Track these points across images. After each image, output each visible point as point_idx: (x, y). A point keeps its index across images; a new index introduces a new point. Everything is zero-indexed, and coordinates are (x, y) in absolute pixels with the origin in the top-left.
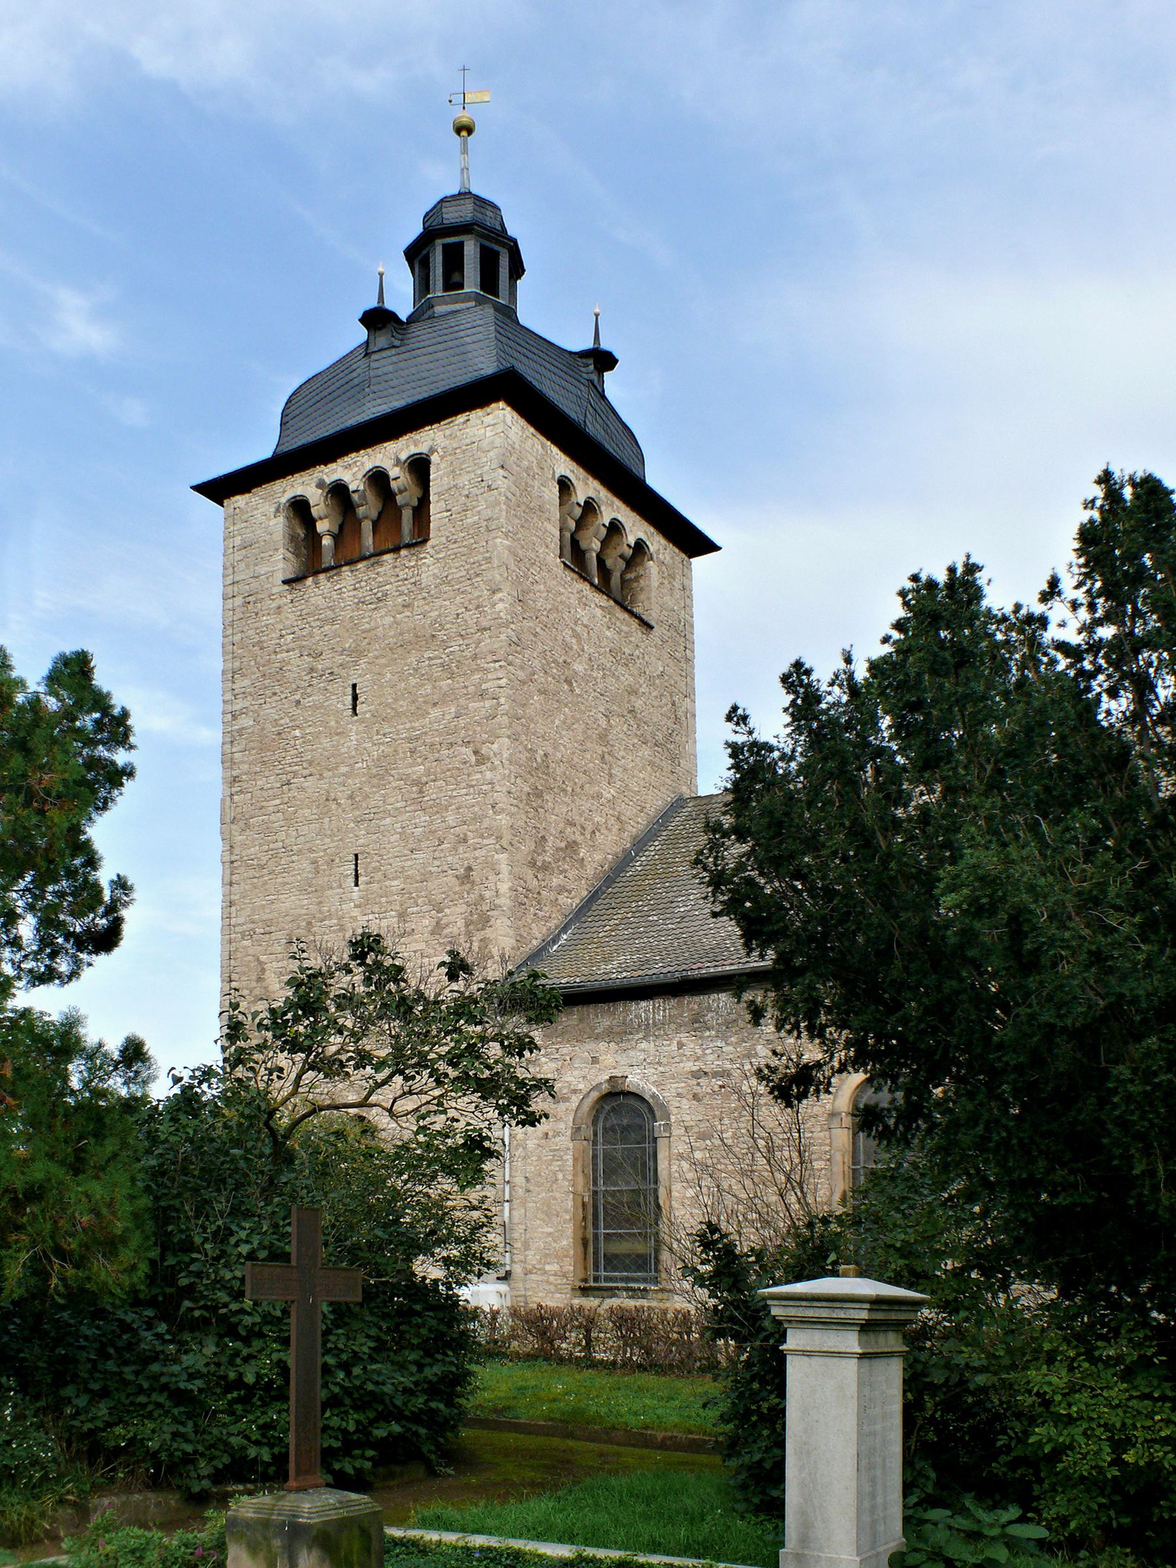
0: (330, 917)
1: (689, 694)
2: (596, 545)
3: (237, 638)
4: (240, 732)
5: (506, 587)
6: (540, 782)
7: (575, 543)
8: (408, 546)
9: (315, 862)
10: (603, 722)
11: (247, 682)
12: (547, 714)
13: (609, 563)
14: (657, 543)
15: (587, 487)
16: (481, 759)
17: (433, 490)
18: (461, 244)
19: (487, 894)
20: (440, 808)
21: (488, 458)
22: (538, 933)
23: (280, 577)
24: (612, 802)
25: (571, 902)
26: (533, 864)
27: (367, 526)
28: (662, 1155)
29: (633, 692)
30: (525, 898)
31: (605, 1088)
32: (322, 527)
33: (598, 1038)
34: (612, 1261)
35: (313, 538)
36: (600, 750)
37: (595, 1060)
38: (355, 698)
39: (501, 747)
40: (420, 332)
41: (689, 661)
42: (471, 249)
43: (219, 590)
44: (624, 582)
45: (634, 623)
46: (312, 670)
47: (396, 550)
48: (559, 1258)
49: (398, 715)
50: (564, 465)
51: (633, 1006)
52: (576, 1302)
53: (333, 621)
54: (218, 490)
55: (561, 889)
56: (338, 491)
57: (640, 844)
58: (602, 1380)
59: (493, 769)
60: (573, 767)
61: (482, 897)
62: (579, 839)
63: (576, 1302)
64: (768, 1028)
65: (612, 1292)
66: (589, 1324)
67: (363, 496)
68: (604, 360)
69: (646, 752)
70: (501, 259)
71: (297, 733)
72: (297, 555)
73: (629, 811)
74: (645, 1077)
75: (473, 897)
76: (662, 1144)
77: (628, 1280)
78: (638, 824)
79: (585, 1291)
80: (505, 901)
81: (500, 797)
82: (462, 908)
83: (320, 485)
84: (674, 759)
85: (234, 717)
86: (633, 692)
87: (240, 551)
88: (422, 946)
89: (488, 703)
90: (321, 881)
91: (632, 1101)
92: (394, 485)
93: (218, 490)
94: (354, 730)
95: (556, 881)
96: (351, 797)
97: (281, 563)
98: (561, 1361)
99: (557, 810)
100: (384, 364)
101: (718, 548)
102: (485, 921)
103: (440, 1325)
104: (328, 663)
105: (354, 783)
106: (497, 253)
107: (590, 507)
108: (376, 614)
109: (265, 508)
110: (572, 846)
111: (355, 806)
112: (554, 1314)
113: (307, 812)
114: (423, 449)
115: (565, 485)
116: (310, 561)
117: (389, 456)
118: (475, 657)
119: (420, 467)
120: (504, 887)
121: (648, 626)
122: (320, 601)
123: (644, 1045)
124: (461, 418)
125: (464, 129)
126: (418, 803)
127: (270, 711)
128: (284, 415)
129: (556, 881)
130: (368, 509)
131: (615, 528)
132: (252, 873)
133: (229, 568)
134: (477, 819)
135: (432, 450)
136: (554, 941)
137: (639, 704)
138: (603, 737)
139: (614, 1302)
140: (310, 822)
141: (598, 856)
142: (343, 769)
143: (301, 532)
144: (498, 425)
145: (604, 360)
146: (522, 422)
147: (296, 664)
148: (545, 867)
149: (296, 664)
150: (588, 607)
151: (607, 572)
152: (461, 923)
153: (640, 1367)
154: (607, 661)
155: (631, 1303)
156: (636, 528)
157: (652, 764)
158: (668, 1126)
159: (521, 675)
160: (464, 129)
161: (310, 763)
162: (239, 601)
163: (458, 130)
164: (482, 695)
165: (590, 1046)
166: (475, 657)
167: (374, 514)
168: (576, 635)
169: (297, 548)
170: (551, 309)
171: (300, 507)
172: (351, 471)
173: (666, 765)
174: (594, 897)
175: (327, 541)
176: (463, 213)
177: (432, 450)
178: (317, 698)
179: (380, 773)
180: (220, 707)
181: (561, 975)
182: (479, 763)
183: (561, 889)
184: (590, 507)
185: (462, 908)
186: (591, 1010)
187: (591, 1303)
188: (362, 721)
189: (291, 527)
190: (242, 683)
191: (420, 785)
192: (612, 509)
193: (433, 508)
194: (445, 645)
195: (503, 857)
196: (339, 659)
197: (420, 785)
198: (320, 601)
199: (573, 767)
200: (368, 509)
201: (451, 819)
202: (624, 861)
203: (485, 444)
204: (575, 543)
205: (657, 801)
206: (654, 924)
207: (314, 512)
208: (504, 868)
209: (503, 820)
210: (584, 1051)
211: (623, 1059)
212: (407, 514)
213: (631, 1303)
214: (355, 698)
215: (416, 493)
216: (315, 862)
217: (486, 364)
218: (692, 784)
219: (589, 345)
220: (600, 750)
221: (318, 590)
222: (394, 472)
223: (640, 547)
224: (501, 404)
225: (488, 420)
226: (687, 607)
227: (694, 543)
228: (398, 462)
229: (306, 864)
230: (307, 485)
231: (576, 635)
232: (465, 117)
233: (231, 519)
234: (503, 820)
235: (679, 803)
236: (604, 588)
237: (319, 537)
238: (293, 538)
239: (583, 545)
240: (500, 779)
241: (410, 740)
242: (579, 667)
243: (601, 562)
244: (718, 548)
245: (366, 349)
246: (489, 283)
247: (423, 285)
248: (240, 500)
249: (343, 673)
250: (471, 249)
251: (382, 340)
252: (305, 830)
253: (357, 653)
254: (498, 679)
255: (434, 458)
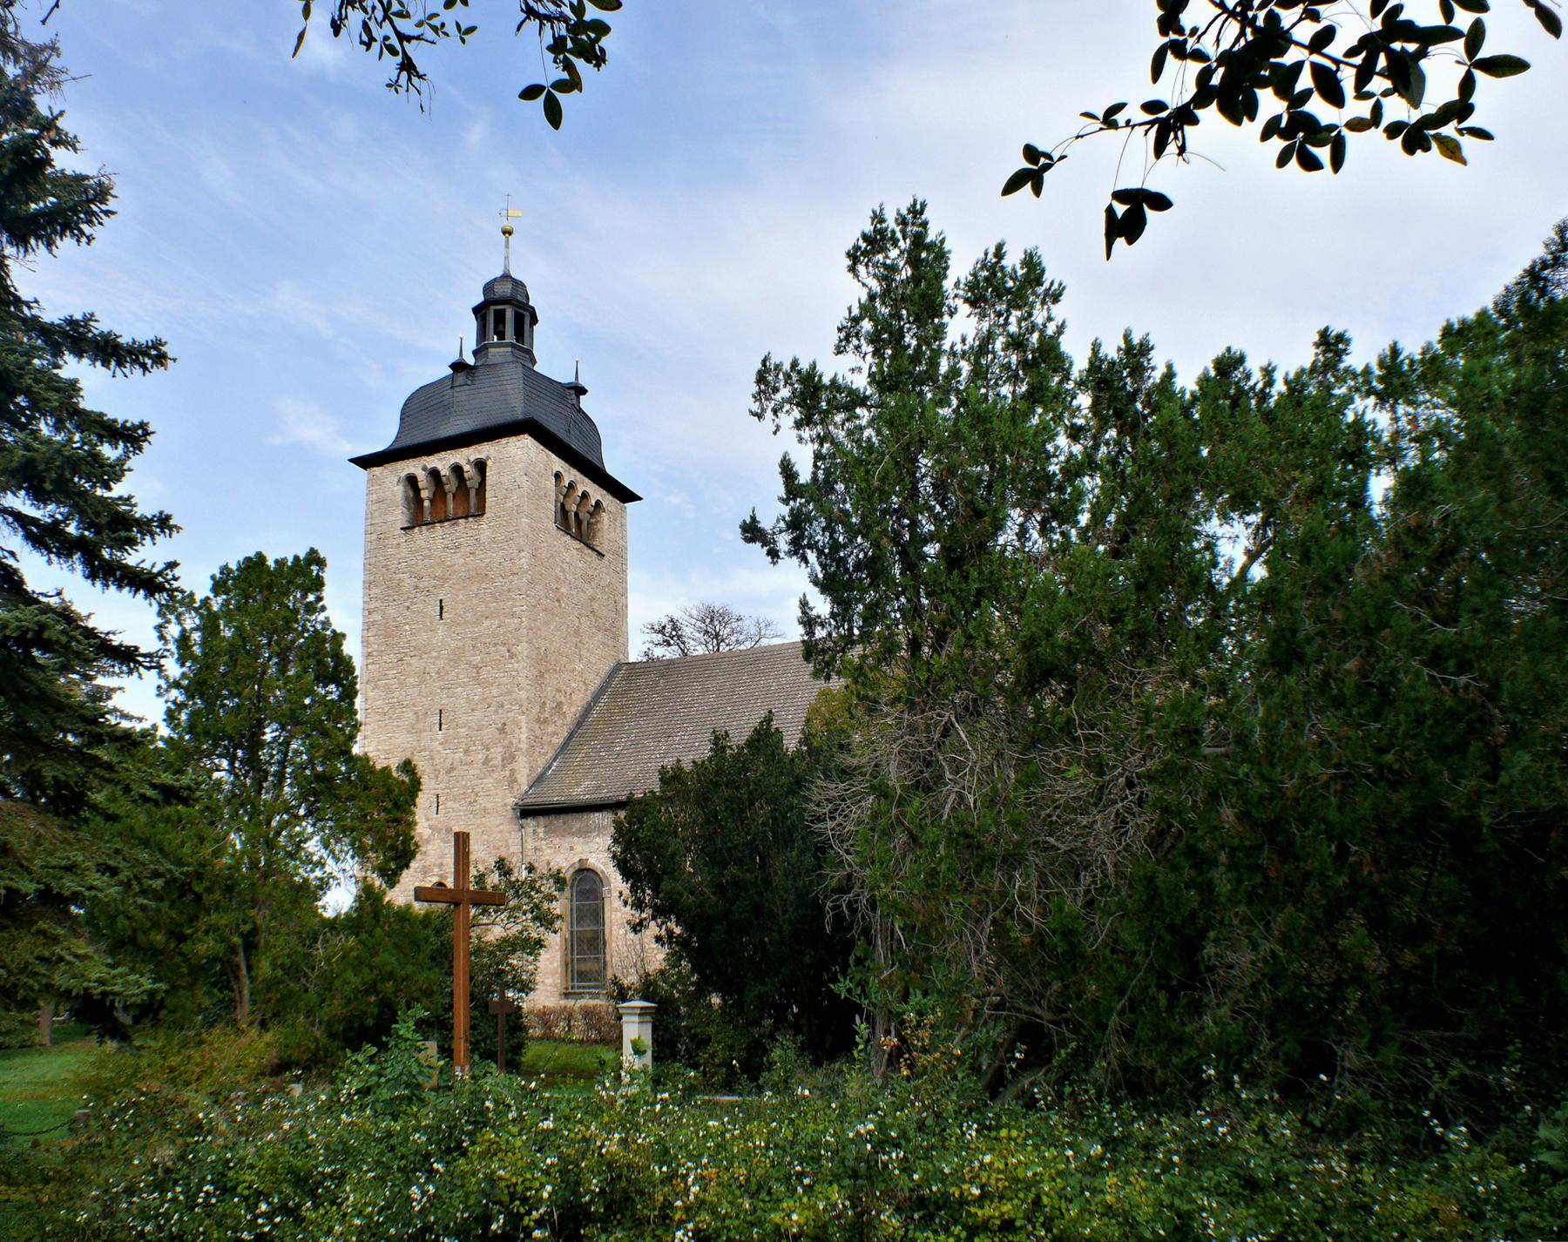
1: (624, 594)
2: (574, 508)
4: (373, 623)
6: (544, 665)
12: (547, 623)
14: (608, 501)
15: (571, 474)
21: (518, 464)
22: (541, 763)
24: (581, 672)
25: (558, 741)
27: (450, 497)
28: (607, 909)
29: (593, 599)
30: (535, 742)
31: (577, 866)
32: (424, 494)
33: (573, 834)
35: (418, 501)
37: (572, 849)
39: (522, 648)
41: (624, 572)
42: (510, 314)
47: (466, 517)
49: (466, 622)
50: (558, 464)
52: (563, 1002)
53: (430, 557)
54: (365, 462)
55: (554, 734)
56: (434, 474)
57: (596, 698)
58: (577, 1049)
63: (563, 1002)
65: (580, 995)
66: (569, 1016)
68: (581, 391)
69: (600, 636)
70: (526, 317)
73: (590, 677)
76: (607, 901)
78: (595, 683)
79: (567, 995)
80: (524, 746)
81: (521, 679)
83: (424, 468)
86: (593, 599)
87: (378, 503)
93: (365, 462)
94: (441, 629)
97: (400, 516)
99: (552, 681)
100: (462, 395)
102: (513, 758)
103: (514, 1020)
105: (441, 663)
107: (571, 486)
109: (392, 477)
110: (560, 705)
111: (441, 678)
112: (553, 1011)
115: (558, 476)
117: (464, 457)
119: (481, 466)
120: (523, 737)
121: (601, 555)
122: (422, 543)
124: (504, 441)
125: (507, 232)
126: (476, 680)
127: (391, 611)
128: (403, 412)
130: (451, 486)
131: (585, 495)
133: (369, 515)
134: (510, 692)
137: (596, 606)
138: (577, 632)
139: (582, 1002)
141: (572, 710)
143: (411, 494)
144: (523, 448)
145: (581, 391)
147: (408, 582)
148: (545, 721)
149: (408, 582)
150: (569, 548)
151: (577, 523)
153: (596, 1041)
155: (592, 1002)
156: (596, 493)
159: (534, 602)
160: (507, 232)
162: (374, 536)
164: (513, 615)
165: (569, 839)
168: (563, 571)
170: (553, 356)
171: (412, 480)
172: (442, 462)
174: (571, 736)
175: (426, 504)
176: (504, 290)
179: (456, 658)
180: (361, 604)
182: (511, 657)
183: (554, 734)
184: (571, 486)
186: (570, 818)
187: (570, 1003)
190: (375, 591)
192: (585, 485)
193: (488, 494)
196: (434, 582)
198: (422, 543)
200: (451, 486)
201: (495, 692)
202: (588, 710)
205: (605, 668)
206: (603, 758)
207: (420, 485)
208: (524, 725)
209: (523, 694)
210: (565, 842)
211: (586, 849)
212: (473, 493)
213: (592, 1002)
215: (479, 479)
218: (626, 653)
221: (421, 535)
222: (466, 468)
223: (598, 503)
228: (469, 462)
230: (415, 467)
231: (563, 571)
232: (507, 225)
233: (371, 482)
234: (523, 694)
236: (579, 537)
237: (422, 501)
238: (407, 498)
240: (522, 668)
242: (564, 590)
243: (576, 514)
245: (452, 378)
246: (519, 333)
247: (482, 333)
248: (377, 470)
250: (510, 314)
251: (461, 378)
252: (411, 691)
253: (443, 579)
254: (521, 607)
255: (489, 463)
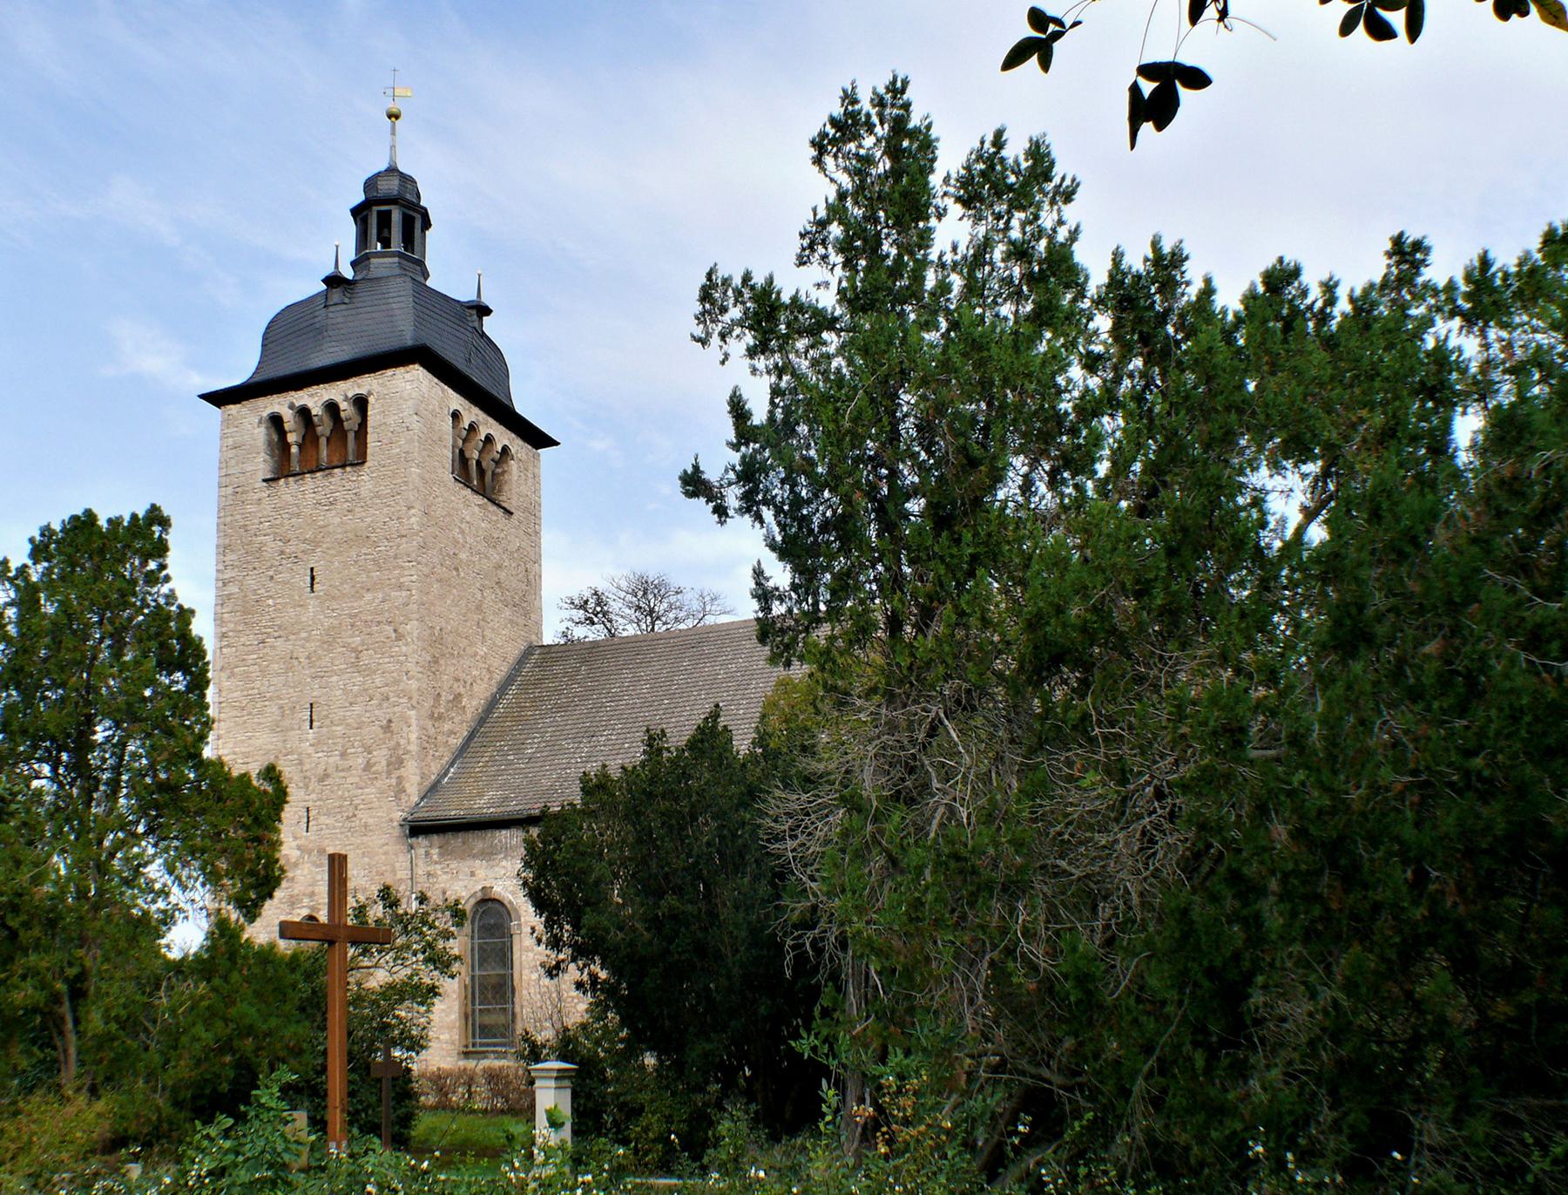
0: (291, 753)
2: (476, 455)
3: (229, 519)
4: (229, 596)
5: (417, 505)
6: (438, 648)
7: (462, 452)
8: (352, 465)
9: (281, 707)
10: (479, 596)
11: (234, 557)
12: (442, 597)
13: (484, 464)
14: (518, 446)
15: (471, 414)
16: (399, 637)
17: (370, 423)
18: (390, 212)
19: (402, 742)
20: (370, 672)
21: (407, 401)
22: (435, 768)
23: (261, 476)
24: (484, 657)
25: (456, 742)
26: (432, 716)
27: (323, 441)
29: (499, 567)
31: (479, 896)
32: (291, 438)
33: (474, 857)
34: (485, 1031)
35: (284, 446)
36: (476, 617)
37: (473, 874)
38: (313, 578)
39: (412, 628)
40: (363, 294)
41: (537, 533)
42: (396, 216)
43: (216, 480)
44: (494, 474)
45: (500, 512)
46: (282, 552)
47: (343, 466)
48: (450, 1029)
50: (456, 401)
51: (497, 833)
52: (462, 1063)
53: (298, 515)
54: (218, 398)
55: (451, 733)
56: (304, 412)
57: (503, 688)
59: (407, 644)
60: (458, 635)
61: (398, 744)
62: (462, 690)
63: (462, 1063)
64: (543, 946)
67: (321, 420)
68: (484, 311)
69: (507, 612)
70: (416, 220)
71: (270, 602)
72: (272, 456)
73: (496, 663)
74: (505, 888)
75: (393, 743)
77: (495, 1045)
79: (466, 1055)
80: (413, 748)
82: (385, 752)
83: (292, 406)
84: (526, 614)
85: (225, 584)
86: (499, 567)
87: (234, 450)
88: (356, 780)
89: (404, 594)
90: (286, 723)
91: (496, 905)
92: (343, 415)
93: (218, 398)
94: (312, 604)
95: (447, 726)
96: (308, 658)
97: (261, 464)
98: (453, 1110)
99: (449, 669)
100: (337, 315)
101: (557, 444)
104: (293, 549)
105: (311, 646)
106: (413, 218)
107: (472, 428)
108: (329, 514)
109: (252, 417)
110: (458, 697)
111: (311, 665)
112: (449, 1074)
113: (276, 666)
114: (363, 391)
115: (456, 416)
116: (283, 467)
117: (341, 392)
118: (396, 557)
119: (361, 403)
120: (413, 737)
123: (504, 863)
124: (389, 372)
125: (393, 116)
126: (356, 666)
127: (251, 582)
128: (265, 338)
129: (447, 726)
130: (324, 429)
131: (489, 439)
132: (235, 713)
133: (224, 463)
134: (397, 682)
135: (370, 393)
136: (445, 774)
137: (503, 575)
138: (479, 608)
139: (485, 1063)
140: (279, 675)
142: (304, 635)
143: (275, 437)
144: (414, 381)
145: (484, 311)
146: (430, 376)
148: (440, 717)
149: (272, 546)
150: (469, 504)
152: (384, 763)
154: (482, 547)
156: (503, 437)
157: (511, 621)
158: (519, 925)
159: (426, 570)
160: (393, 116)
161: (280, 627)
162: (230, 490)
163: (390, 116)
164: (400, 587)
165: (469, 862)
166: (396, 557)
167: (328, 433)
168: (462, 532)
169: (272, 450)
171: (276, 421)
172: (314, 398)
173: (521, 621)
175: (294, 449)
176: (390, 186)
177: (370, 393)
178: (286, 576)
180: (214, 574)
181: (453, 809)
182: (398, 639)
183: (451, 733)
184: (472, 428)
185: (385, 752)
187: (471, 1064)
188: (317, 598)
189: (269, 435)
190: (231, 557)
191: (357, 652)
192: (489, 426)
194: (375, 545)
195: (413, 713)
197: (357, 652)
198: (288, 498)
199: (458, 635)
200: (324, 429)
201: (378, 681)
203: (405, 394)
204: (462, 452)
205: (514, 652)
206: (511, 763)
207: (287, 427)
208: (414, 722)
209: (414, 684)
210: (465, 866)
212: (351, 436)
214: (313, 578)
215: (358, 420)
216: (281, 707)
217: (405, 333)
218: (539, 634)
219: (474, 297)
220: (476, 617)
221: (288, 489)
222: (343, 405)
223: (505, 449)
224: (417, 366)
225: (408, 376)
226: (537, 491)
227: (538, 439)
228: (346, 399)
229: (275, 709)
230: (280, 404)
231: (462, 532)
233: (226, 422)
235: (530, 650)
237: (288, 446)
238: (270, 443)
239: (467, 455)
240: (412, 652)
241: (351, 616)
243: (479, 463)
244: (557, 444)
245: (325, 295)
246: (408, 240)
247: (362, 240)
248: (233, 409)
249: (305, 557)
250: (396, 216)
252: (275, 681)
254: (411, 577)
255: (371, 400)
